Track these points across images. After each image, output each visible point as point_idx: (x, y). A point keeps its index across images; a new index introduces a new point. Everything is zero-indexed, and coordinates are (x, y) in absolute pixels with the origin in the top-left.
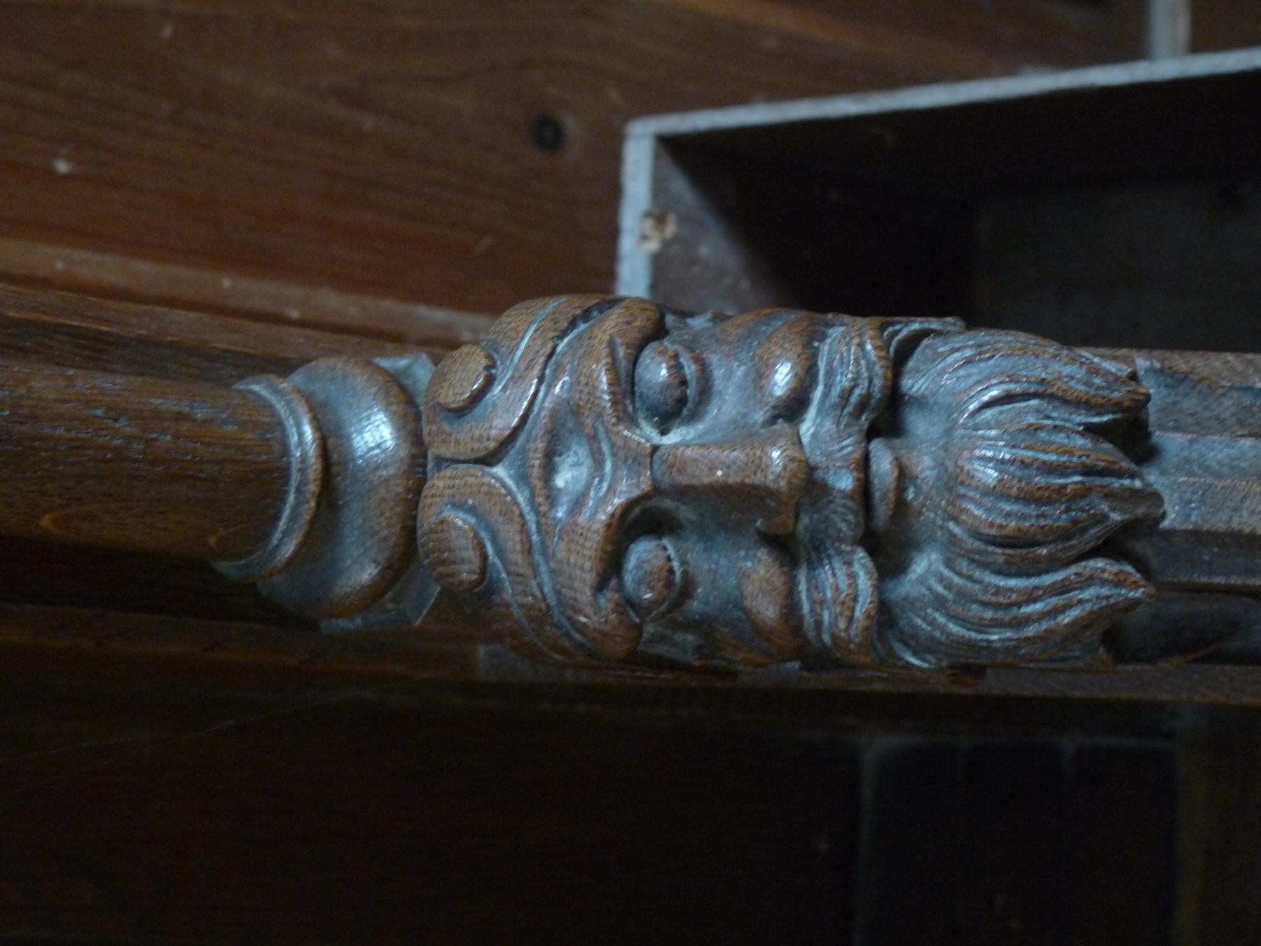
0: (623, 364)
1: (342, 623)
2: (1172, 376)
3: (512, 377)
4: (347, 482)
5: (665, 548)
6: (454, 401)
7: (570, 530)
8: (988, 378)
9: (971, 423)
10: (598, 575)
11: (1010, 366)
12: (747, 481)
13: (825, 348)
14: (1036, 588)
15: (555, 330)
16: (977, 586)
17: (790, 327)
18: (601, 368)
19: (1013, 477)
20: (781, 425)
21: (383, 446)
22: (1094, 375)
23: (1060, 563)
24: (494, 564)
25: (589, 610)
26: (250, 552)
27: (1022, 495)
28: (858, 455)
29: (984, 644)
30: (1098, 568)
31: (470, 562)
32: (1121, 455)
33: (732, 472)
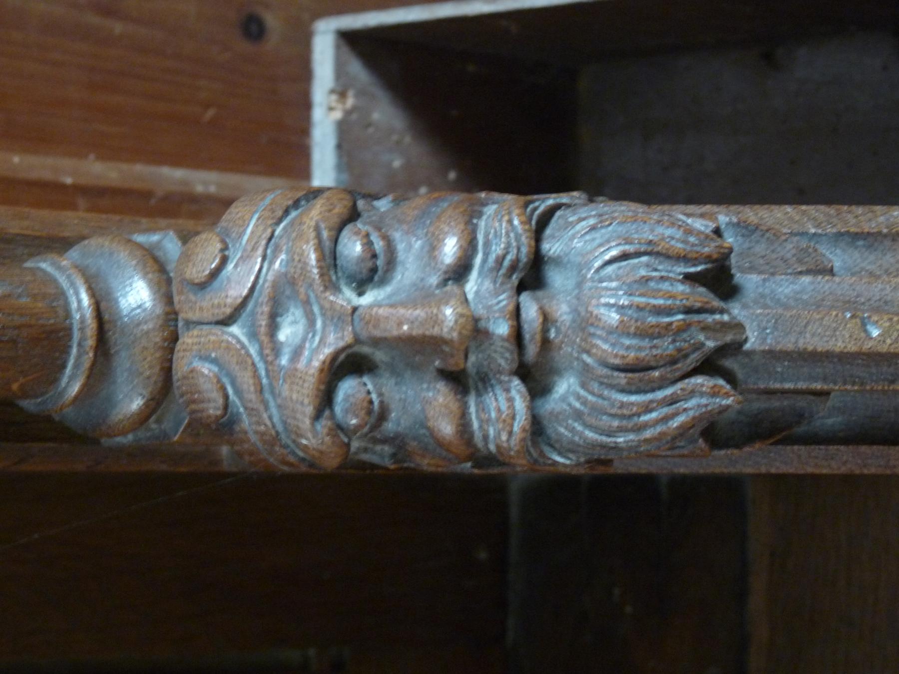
0: (327, 244)
1: (119, 439)
2: (746, 227)
3: (241, 257)
4: (117, 335)
5: (365, 384)
6: (197, 278)
7: (292, 374)
8: (608, 241)
9: (597, 277)
10: (314, 408)
11: (624, 231)
12: (427, 333)
13: (482, 224)
14: (651, 401)
15: (273, 218)
16: (606, 403)
17: (455, 208)
18: (310, 248)
19: (631, 319)
20: (451, 287)
21: (143, 307)
22: (690, 235)
23: (668, 382)
24: (234, 401)
25: (310, 435)
26: (46, 393)
27: (639, 332)
28: (511, 307)
29: (613, 445)
30: (698, 384)
31: (215, 401)
32: (711, 296)
33: (415, 326)
